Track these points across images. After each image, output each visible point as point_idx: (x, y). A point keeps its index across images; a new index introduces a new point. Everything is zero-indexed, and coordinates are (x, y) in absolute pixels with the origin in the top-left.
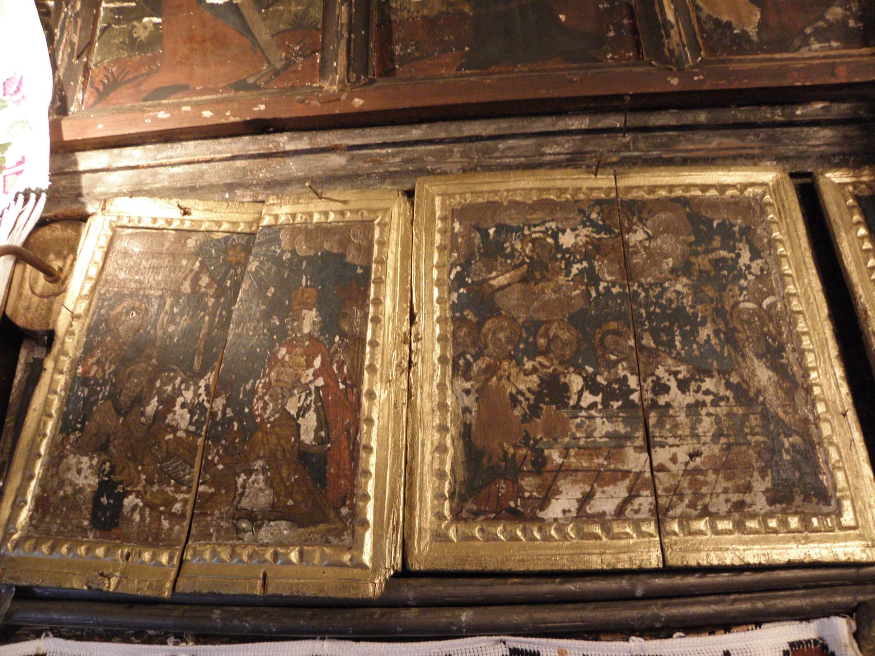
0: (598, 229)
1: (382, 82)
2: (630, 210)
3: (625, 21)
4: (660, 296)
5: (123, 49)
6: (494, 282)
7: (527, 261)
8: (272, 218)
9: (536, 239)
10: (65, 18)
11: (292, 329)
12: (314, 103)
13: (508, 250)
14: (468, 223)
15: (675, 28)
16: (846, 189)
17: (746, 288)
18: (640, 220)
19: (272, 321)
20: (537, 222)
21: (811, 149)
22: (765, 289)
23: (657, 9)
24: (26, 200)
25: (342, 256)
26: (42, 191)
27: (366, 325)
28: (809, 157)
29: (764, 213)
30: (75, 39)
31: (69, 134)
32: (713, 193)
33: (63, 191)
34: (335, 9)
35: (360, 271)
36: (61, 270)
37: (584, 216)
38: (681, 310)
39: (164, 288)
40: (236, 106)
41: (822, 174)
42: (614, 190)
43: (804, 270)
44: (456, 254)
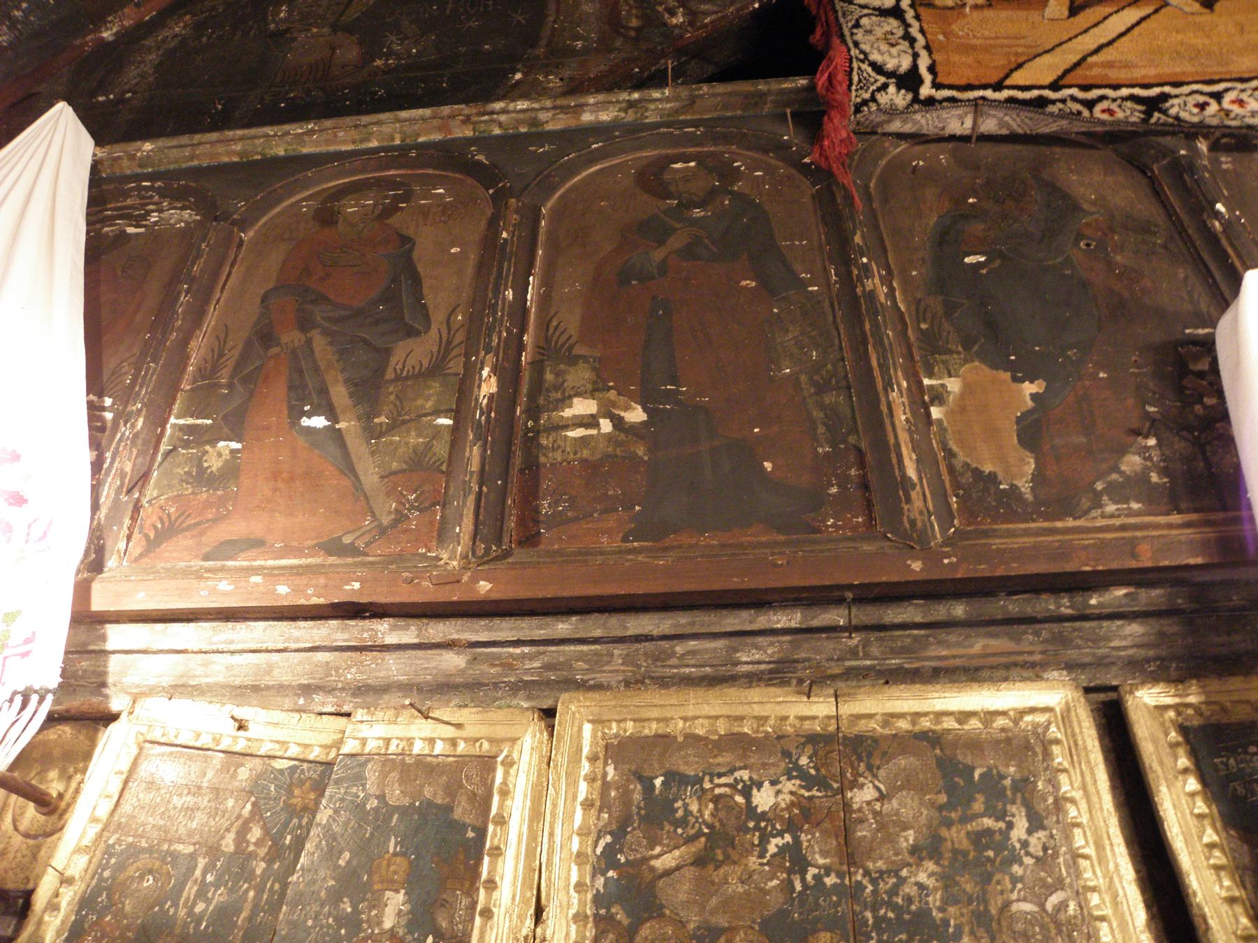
0: (809, 782)
1: (520, 555)
2: (855, 751)
3: (853, 472)
4: (893, 892)
5: (188, 483)
6: (657, 863)
7: (706, 831)
8: (357, 742)
9: (720, 796)
10: (120, 440)
11: (368, 921)
12: (426, 584)
13: (680, 813)
14: (626, 767)
15: (918, 488)
16: (1166, 717)
17: (1021, 879)
18: (870, 768)
19: (342, 906)
20: (723, 770)
21: (1114, 653)
22: (1049, 880)
23: (894, 460)
24: (24, 705)
25: (449, 809)
26: (48, 691)
27: (472, 920)
28: (1113, 663)
29: (1047, 755)
30: (128, 468)
31: (99, 603)
32: (974, 724)
33: (82, 678)
34: (464, 448)
35: (471, 834)
36: (61, 796)
37: (790, 762)
38: (924, 913)
39: (198, 843)
40: (322, 581)
41: (1131, 692)
42: (833, 721)
43: (1108, 848)
44: (606, 816)
